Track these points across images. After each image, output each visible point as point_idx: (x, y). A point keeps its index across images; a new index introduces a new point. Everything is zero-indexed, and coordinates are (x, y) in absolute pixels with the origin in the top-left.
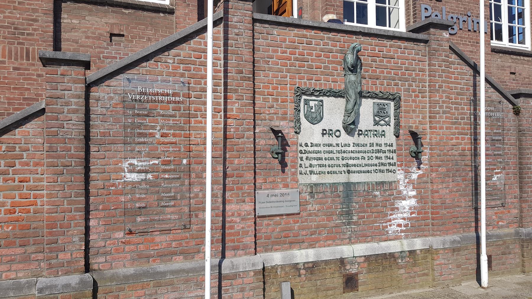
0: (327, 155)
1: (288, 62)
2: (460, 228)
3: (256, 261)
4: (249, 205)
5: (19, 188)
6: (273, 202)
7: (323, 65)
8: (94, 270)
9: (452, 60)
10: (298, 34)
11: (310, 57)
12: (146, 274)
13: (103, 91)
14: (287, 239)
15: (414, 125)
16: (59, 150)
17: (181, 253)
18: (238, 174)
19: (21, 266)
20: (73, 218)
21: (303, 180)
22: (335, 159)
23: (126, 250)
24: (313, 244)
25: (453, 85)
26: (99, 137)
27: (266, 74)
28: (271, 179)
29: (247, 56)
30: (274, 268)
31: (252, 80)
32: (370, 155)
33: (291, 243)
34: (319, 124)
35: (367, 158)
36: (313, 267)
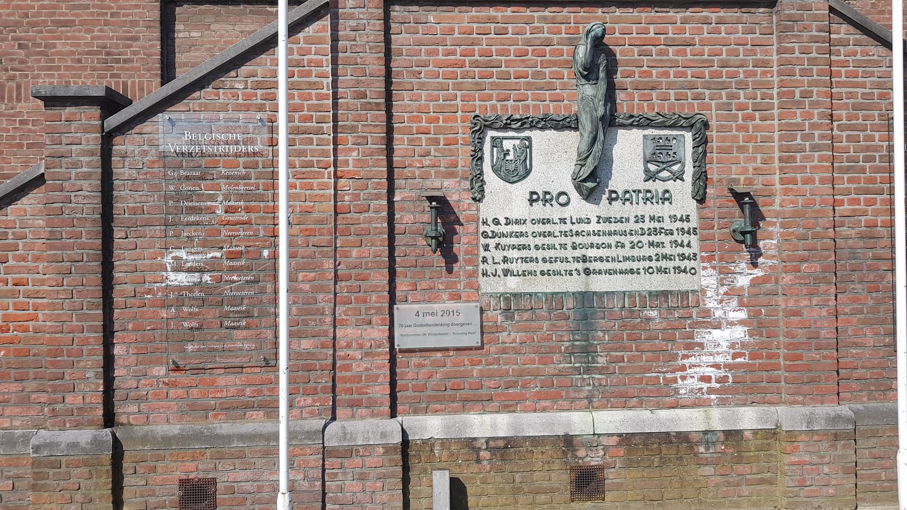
0: (539, 241)
1: (459, 70)
2: (861, 391)
3: (389, 429)
4: (379, 330)
5: (13, 295)
6: (427, 325)
7: (530, 70)
8: (122, 424)
9: (842, 36)
10: (478, 17)
11: (503, 58)
12: (197, 437)
13: (133, 143)
14: (458, 393)
15: (742, 178)
16: (64, 236)
17: (260, 407)
18: (359, 275)
19: (17, 410)
20: (85, 342)
21: (488, 286)
22: (558, 246)
23: (170, 395)
24: (511, 406)
25: (844, 90)
26: (126, 216)
27: (413, 95)
28: (424, 284)
29: (374, 67)
30: (429, 444)
31: (384, 108)
32: (635, 239)
33: (465, 400)
34: (524, 181)
35: (628, 245)
36: (506, 447)
